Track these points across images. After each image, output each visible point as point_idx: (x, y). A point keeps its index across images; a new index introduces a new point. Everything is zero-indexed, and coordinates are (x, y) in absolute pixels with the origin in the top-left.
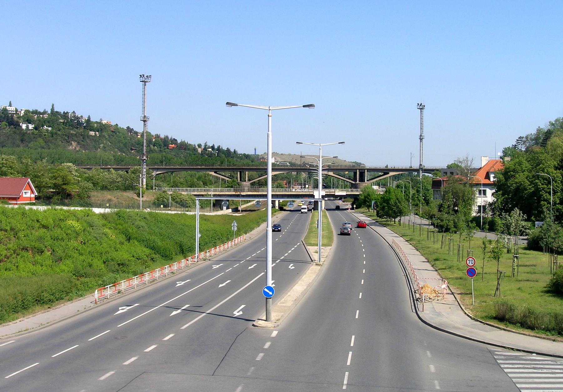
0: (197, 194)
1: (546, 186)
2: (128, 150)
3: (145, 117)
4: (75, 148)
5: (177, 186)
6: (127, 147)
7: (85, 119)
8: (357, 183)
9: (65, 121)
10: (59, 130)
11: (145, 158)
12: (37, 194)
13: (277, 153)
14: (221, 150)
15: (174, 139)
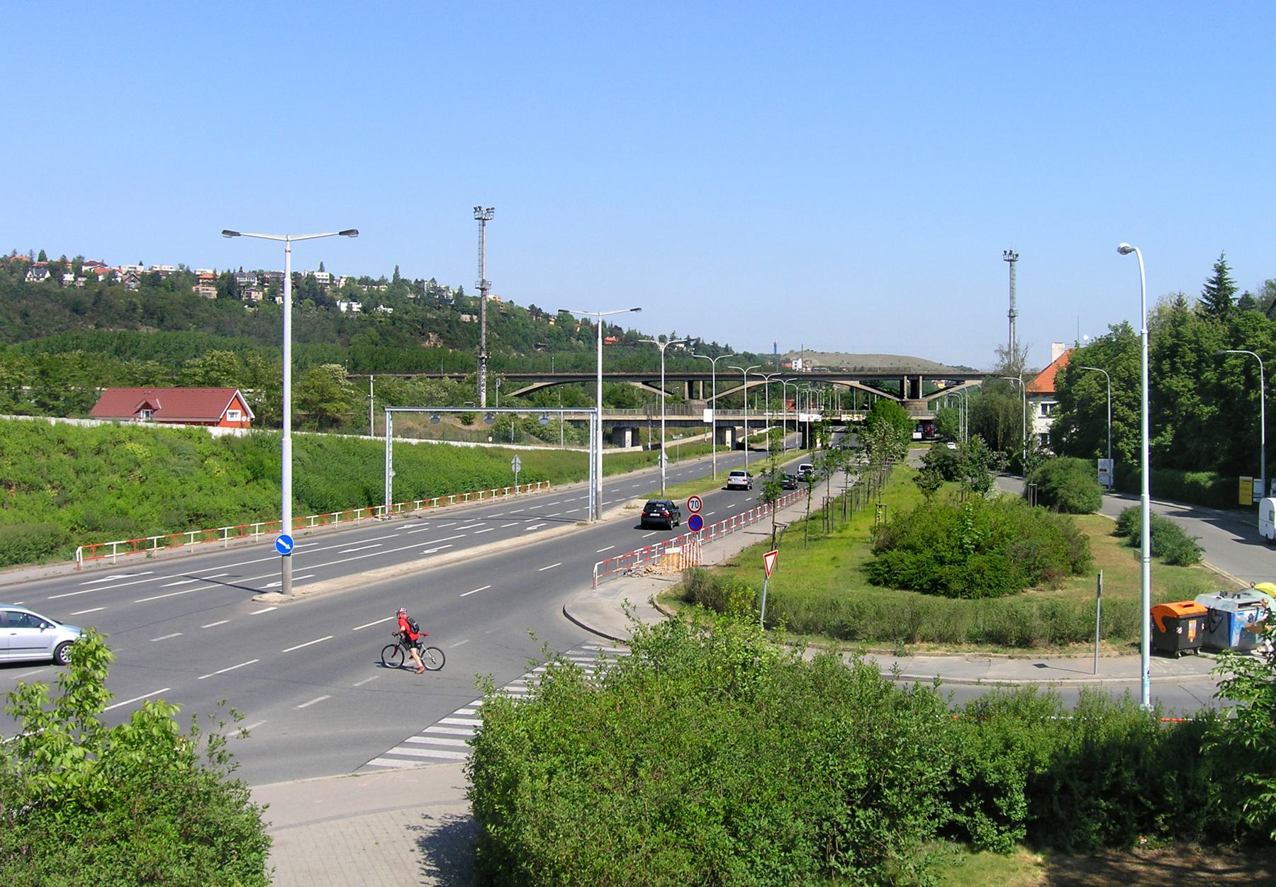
1: (1123, 393)
2: (530, 347)
3: (483, 281)
4: (436, 344)
6: (529, 342)
7: (454, 292)
9: (417, 296)
10: (407, 313)
11: (483, 355)
12: (253, 416)
15: (616, 326)
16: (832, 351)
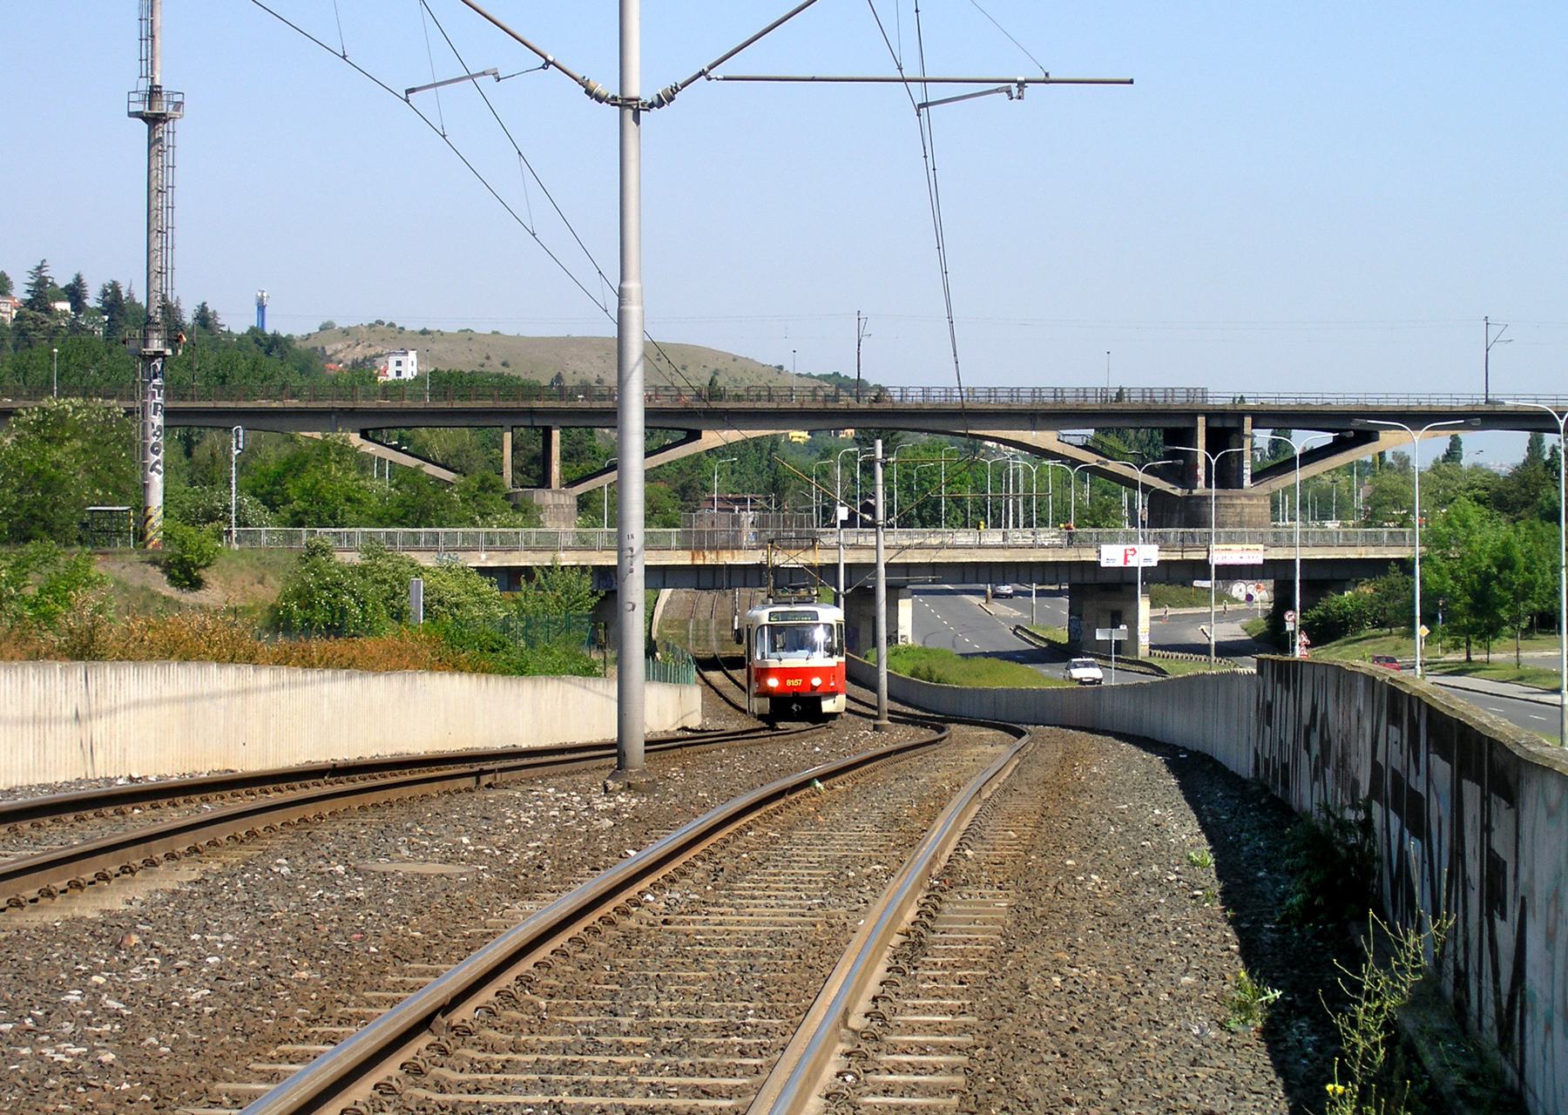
0: (490, 564)
3: (154, 93)
5: (333, 517)
8: (1195, 492)
11: (156, 345)
13: (398, 325)
14: (128, 311)
16: (451, 328)
